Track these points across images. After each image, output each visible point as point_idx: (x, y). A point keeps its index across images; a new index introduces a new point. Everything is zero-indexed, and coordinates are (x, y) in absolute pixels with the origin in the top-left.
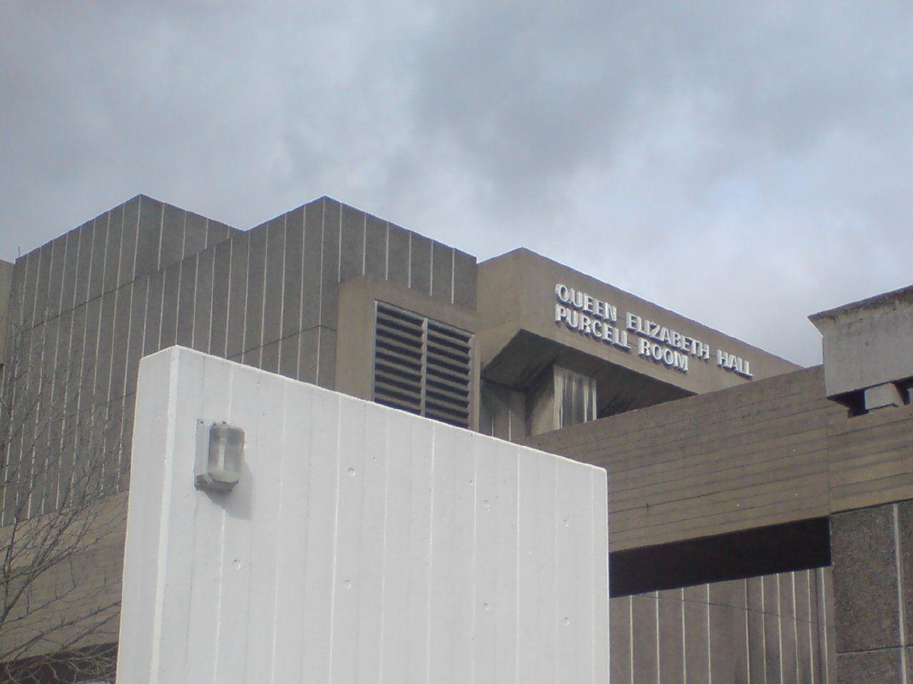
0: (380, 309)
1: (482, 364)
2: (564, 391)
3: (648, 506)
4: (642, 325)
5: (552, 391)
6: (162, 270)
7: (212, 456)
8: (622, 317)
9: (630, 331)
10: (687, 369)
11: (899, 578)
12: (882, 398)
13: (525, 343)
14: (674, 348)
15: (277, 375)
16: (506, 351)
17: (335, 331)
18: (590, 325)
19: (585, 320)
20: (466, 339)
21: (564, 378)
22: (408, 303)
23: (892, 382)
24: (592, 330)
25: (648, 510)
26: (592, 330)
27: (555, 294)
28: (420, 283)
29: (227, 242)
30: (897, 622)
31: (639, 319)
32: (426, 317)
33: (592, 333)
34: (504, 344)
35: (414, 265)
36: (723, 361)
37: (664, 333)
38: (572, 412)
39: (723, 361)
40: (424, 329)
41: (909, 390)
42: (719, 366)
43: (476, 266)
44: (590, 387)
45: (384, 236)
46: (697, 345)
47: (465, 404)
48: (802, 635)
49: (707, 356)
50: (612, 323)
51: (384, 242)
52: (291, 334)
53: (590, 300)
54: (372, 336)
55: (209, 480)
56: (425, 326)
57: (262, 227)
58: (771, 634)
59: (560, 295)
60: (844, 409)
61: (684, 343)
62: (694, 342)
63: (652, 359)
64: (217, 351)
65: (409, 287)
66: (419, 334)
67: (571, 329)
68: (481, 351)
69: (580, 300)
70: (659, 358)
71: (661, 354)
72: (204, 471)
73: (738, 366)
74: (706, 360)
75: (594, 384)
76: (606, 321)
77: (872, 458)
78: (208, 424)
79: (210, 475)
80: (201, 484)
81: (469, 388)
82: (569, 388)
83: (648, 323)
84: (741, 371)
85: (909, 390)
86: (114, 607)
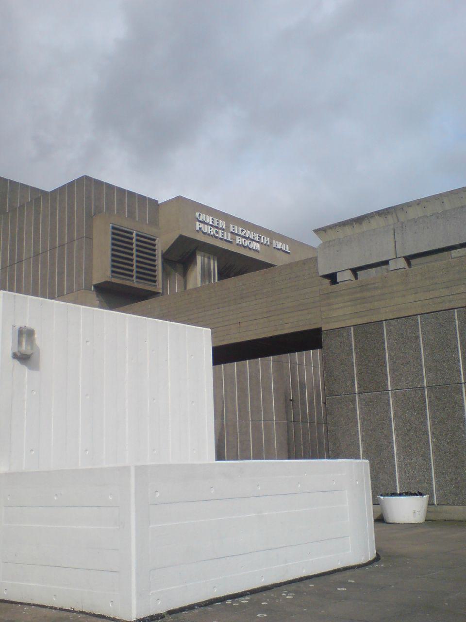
0: (113, 228)
1: (162, 251)
3: (239, 323)
4: (237, 230)
5: (196, 263)
6: (9, 212)
7: (20, 343)
8: (228, 227)
9: (232, 233)
11: (354, 362)
12: (345, 277)
14: (253, 240)
15: (47, 300)
16: (173, 245)
17: (91, 239)
18: (213, 231)
19: (211, 229)
20: (154, 240)
22: (125, 224)
23: (350, 269)
28: (131, 215)
29: (39, 198)
30: (354, 382)
31: (236, 227)
33: (214, 235)
35: (128, 206)
36: (276, 245)
37: (248, 233)
38: (206, 274)
39: (276, 245)
41: (358, 272)
44: (214, 260)
45: (114, 193)
46: (264, 238)
47: (155, 276)
48: (316, 374)
49: (269, 244)
50: (223, 230)
51: (114, 196)
52: (71, 241)
53: (212, 219)
54: (110, 241)
55: (19, 354)
56: (134, 235)
57: (56, 190)
58: (302, 375)
60: (328, 281)
61: (258, 238)
62: (262, 237)
64: (19, 291)
65: (127, 216)
66: (132, 244)
67: (204, 233)
68: (162, 245)
70: (246, 245)
71: (247, 243)
72: (16, 351)
74: (268, 245)
75: (216, 259)
76: (221, 229)
77: (341, 305)
78: (17, 327)
79: (18, 351)
80: (15, 356)
81: (156, 263)
83: (240, 229)
84: (285, 250)
85: (358, 272)
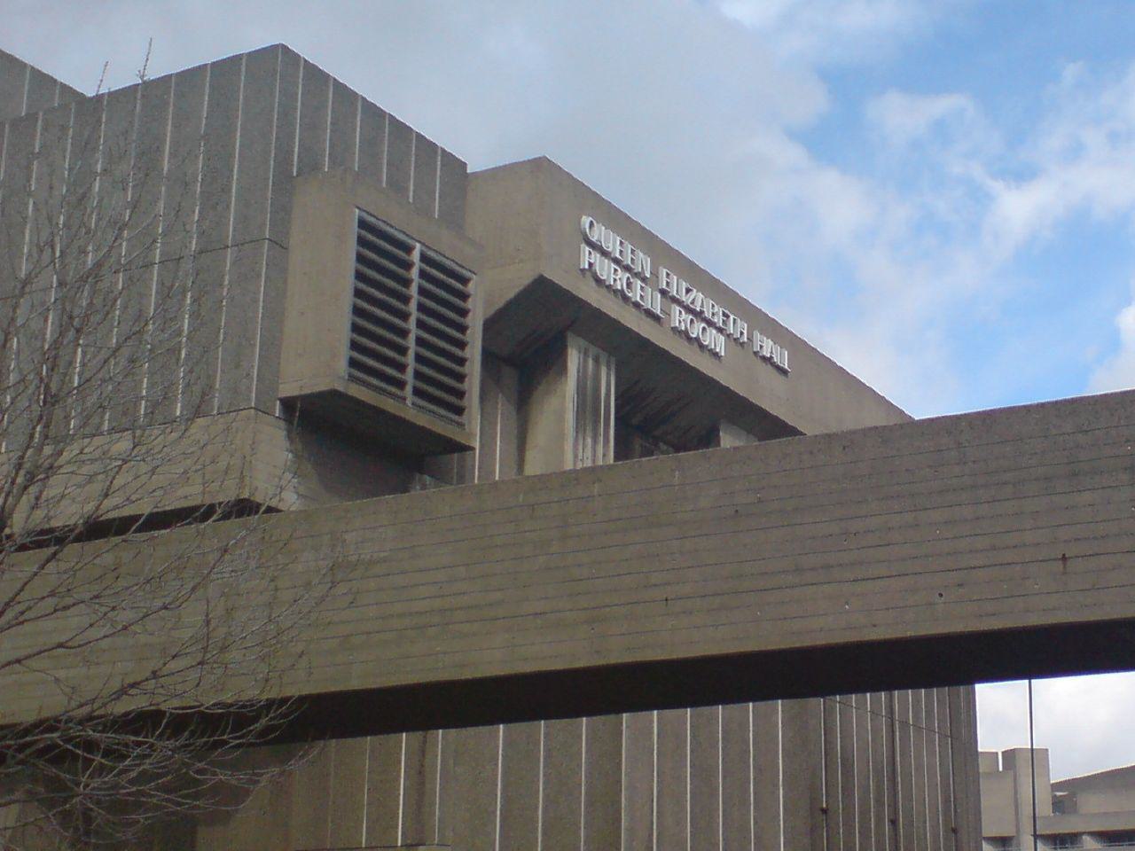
0: (363, 224)
2: (578, 372)
3: (1064, 558)
10: (723, 354)
13: (542, 294)
18: (619, 279)
20: (465, 281)
21: (580, 352)
22: (397, 218)
24: (622, 286)
25: (1065, 565)
26: (622, 286)
27: (580, 229)
32: (419, 242)
33: (622, 291)
34: (511, 295)
37: (698, 299)
40: (415, 261)
42: (756, 353)
43: (466, 175)
44: (609, 369)
46: (734, 320)
59: (588, 230)
62: (732, 317)
63: (685, 335)
69: (607, 240)
70: (694, 336)
71: (696, 330)
73: (777, 357)
75: (613, 360)
82: (585, 367)
86: (139, 680)
